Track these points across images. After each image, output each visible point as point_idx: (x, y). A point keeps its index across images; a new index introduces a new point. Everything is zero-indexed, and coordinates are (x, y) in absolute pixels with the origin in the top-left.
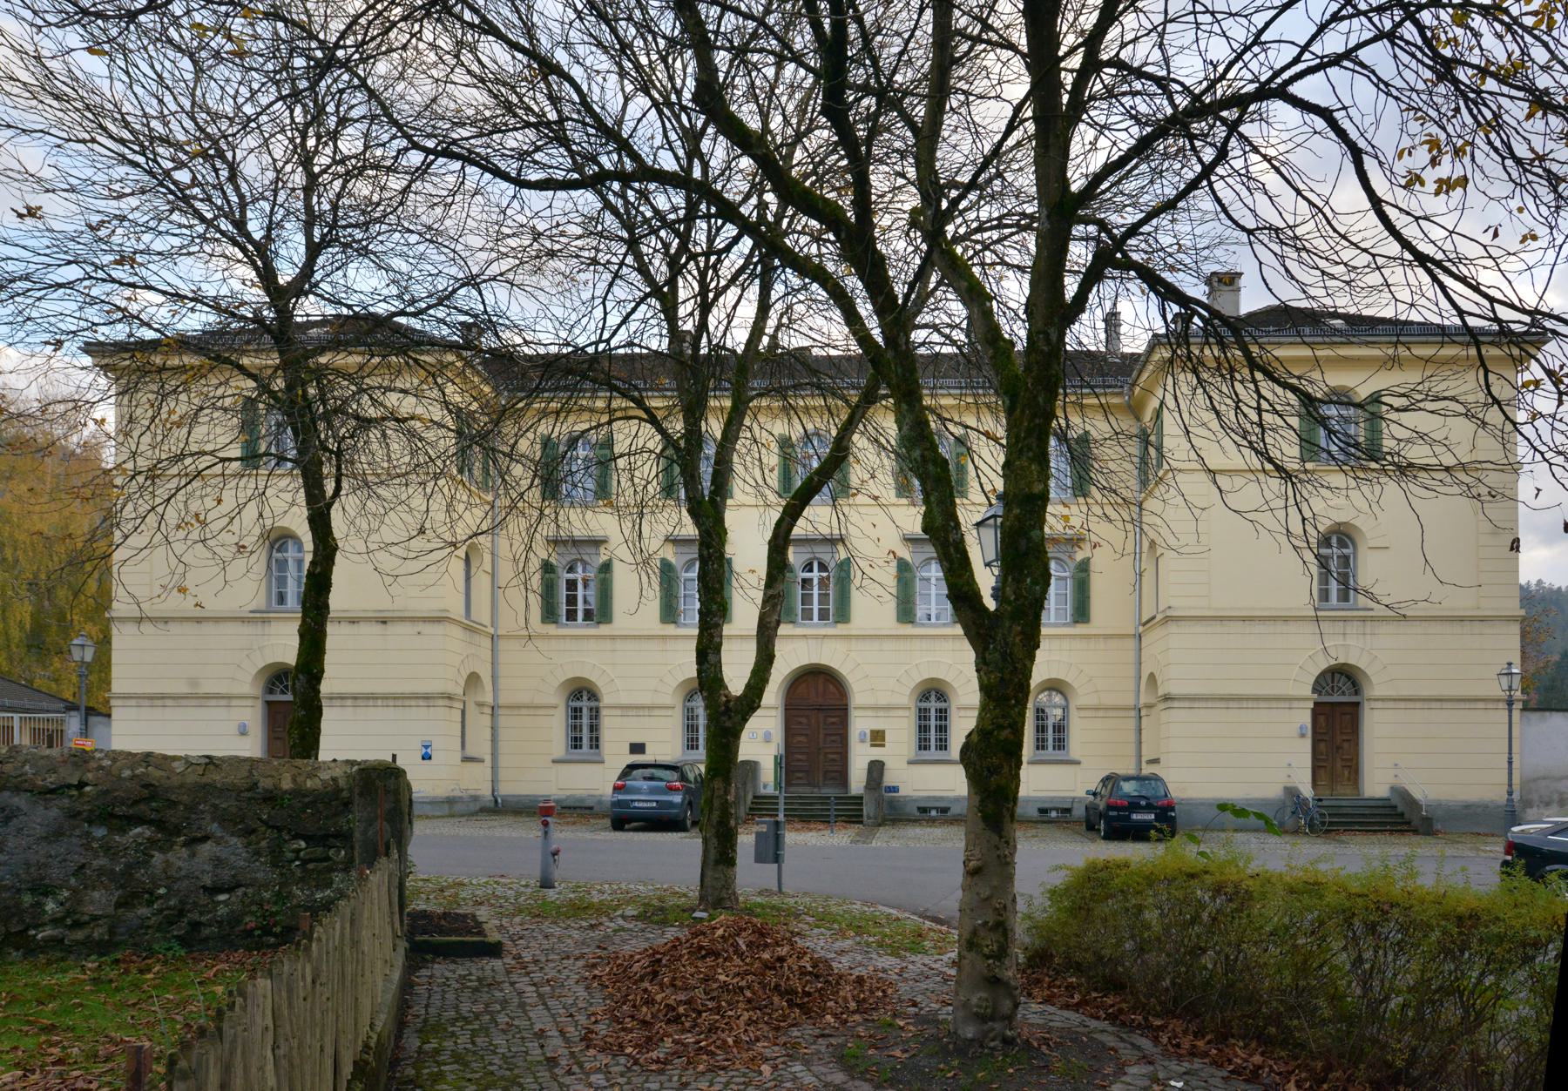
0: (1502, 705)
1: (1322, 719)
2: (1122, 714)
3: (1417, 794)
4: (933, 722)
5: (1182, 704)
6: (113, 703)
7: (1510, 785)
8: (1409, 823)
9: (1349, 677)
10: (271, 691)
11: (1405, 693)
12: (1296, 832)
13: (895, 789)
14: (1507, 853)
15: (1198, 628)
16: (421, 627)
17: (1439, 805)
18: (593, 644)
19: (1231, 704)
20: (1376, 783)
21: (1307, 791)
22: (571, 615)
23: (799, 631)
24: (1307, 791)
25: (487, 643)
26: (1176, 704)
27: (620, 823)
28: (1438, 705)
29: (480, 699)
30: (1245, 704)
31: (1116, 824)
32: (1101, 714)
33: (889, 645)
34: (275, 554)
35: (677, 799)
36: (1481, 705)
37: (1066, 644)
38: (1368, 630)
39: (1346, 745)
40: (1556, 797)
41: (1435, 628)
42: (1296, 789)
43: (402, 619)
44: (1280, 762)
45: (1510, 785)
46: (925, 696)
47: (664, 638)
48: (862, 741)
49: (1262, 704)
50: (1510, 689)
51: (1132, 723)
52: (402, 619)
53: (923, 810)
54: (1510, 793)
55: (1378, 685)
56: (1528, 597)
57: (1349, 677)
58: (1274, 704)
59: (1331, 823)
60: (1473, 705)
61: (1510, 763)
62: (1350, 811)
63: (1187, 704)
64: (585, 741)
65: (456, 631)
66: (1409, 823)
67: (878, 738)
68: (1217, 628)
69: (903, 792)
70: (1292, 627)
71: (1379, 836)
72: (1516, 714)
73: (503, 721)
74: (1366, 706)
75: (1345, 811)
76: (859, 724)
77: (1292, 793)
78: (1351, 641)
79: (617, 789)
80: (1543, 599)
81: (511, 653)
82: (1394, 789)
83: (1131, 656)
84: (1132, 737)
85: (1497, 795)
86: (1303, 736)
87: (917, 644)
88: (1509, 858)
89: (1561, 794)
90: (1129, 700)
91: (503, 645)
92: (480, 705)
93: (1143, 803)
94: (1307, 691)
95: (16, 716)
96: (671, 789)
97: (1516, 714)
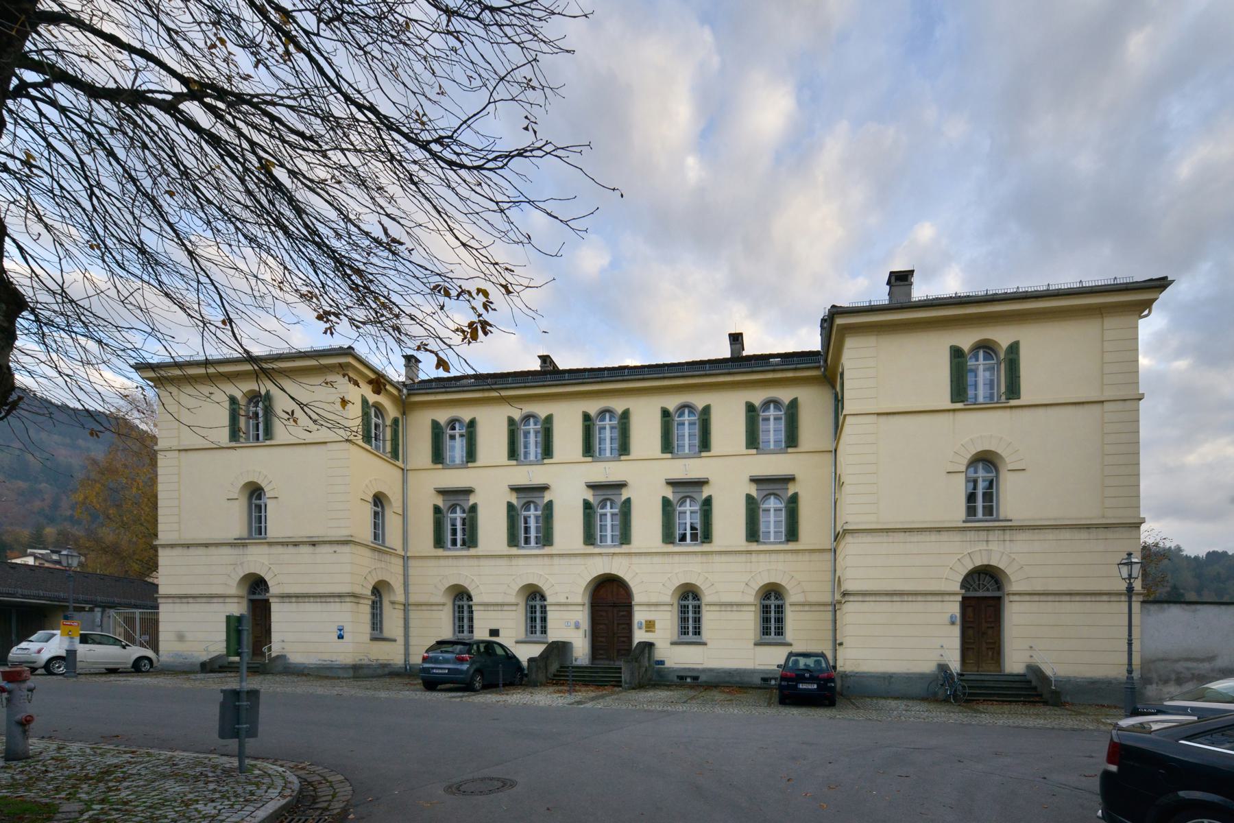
0: (1124, 598)
1: (970, 610)
2: (822, 608)
3: (1048, 672)
4: (691, 615)
5: (856, 598)
6: (160, 600)
7: (1130, 664)
8: (1041, 695)
9: (992, 577)
10: (254, 593)
11: (1039, 587)
12: (946, 701)
13: (662, 663)
14: (1110, 760)
15: (868, 538)
16: (336, 548)
17: (1068, 681)
18: (465, 562)
19: (895, 598)
20: (1015, 661)
21: (955, 666)
22: (454, 543)
23: (597, 550)
24: (955, 666)
25: (400, 562)
26: (851, 598)
27: (431, 684)
28: (1068, 598)
29: (393, 598)
30: (906, 598)
31: (786, 692)
32: (807, 608)
33: (656, 559)
34: (254, 501)
35: (465, 667)
36: (1105, 598)
37: (781, 557)
38: (1007, 537)
39: (990, 632)
40: (1173, 676)
41: (1067, 534)
42: (947, 666)
43: (325, 542)
44: (935, 644)
45: (1130, 664)
46: (684, 596)
47: (510, 556)
48: (640, 628)
49: (920, 598)
50: (1130, 577)
51: (830, 616)
52: (325, 542)
53: (681, 678)
54: (1130, 671)
55: (1016, 583)
56: (1146, 549)
57: (992, 577)
58: (929, 598)
59: (970, 694)
60: (1098, 598)
61: (1130, 644)
62: (991, 684)
63: (860, 598)
64: (538, 628)
65: (367, 553)
66: (1041, 695)
67: (650, 626)
68: (883, 538)
69: (668, 664)
70: (944, 536)
71: (1013, 706)
72: (1136, 607)
73: (413, 615)
74: (1007, 599)
75: (987, 684)
76: (639, 616)
77: (943, 668)
78: (994, 546)
79: (425, 659)
80: (1156, 554)
81: (415, 568)
82: (1029, 667)
83: (828, 566)
84: (830, 626)
85: (1119, 672)
86: (953, 623)
87: (677, 558)
88: (1114, 768)
89: (1178, 673)
90: (827, 598)
91: (411, 563)
92: (393, 603)
93: (807, 675)
94: (956, 587)
95: (137, 611)
96: (462, 660)
97: (1136, 607)
